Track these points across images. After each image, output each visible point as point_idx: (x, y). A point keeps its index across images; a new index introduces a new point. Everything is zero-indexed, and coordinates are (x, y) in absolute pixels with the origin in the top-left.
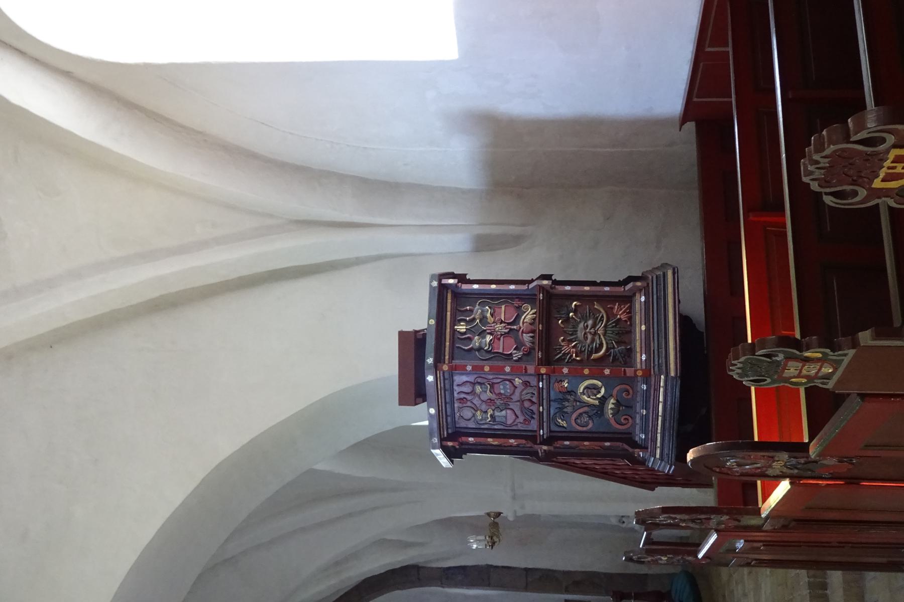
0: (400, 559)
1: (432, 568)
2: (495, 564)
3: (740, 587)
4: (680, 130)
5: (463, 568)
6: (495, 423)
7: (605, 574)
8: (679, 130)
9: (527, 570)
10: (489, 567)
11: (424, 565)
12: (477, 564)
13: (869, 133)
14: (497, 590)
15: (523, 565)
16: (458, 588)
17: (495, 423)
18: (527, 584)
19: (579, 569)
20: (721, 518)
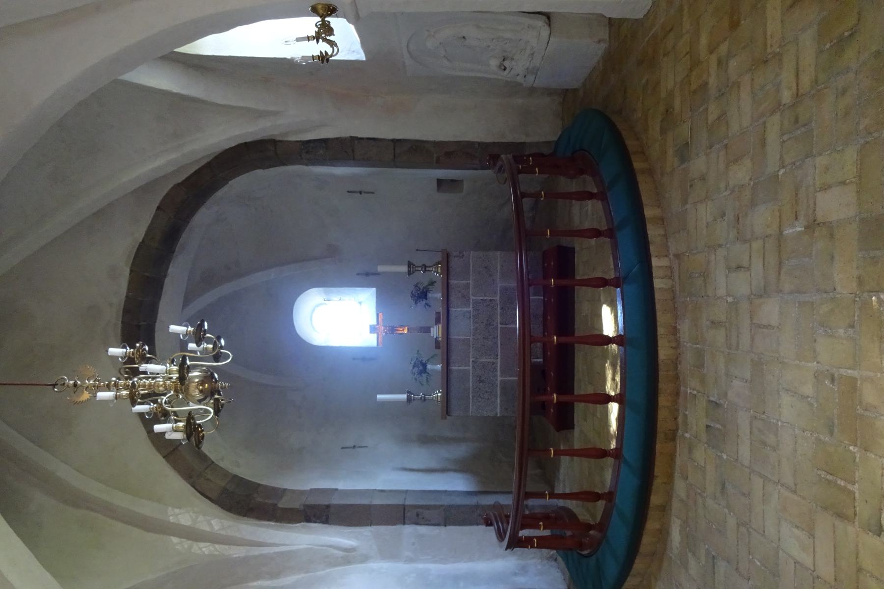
0: (237, 133)
1: (290, 142)
2: (359, 136)
3: (414, 371)
4: (348, 192)
5: (325, 142)
6: (525, 283)
7: (479, 144)
8: (349, 190)
9: (395, 142)
10: (353, 139)
11: (281, 139)
12: (339, 136)
13: (275, 114)
14: (362, 166)
15: (391, 137)
16: (327, 165)
17: (525, 283)
18: (395, 156)
19: (452, 139)
20: (852, 70)
